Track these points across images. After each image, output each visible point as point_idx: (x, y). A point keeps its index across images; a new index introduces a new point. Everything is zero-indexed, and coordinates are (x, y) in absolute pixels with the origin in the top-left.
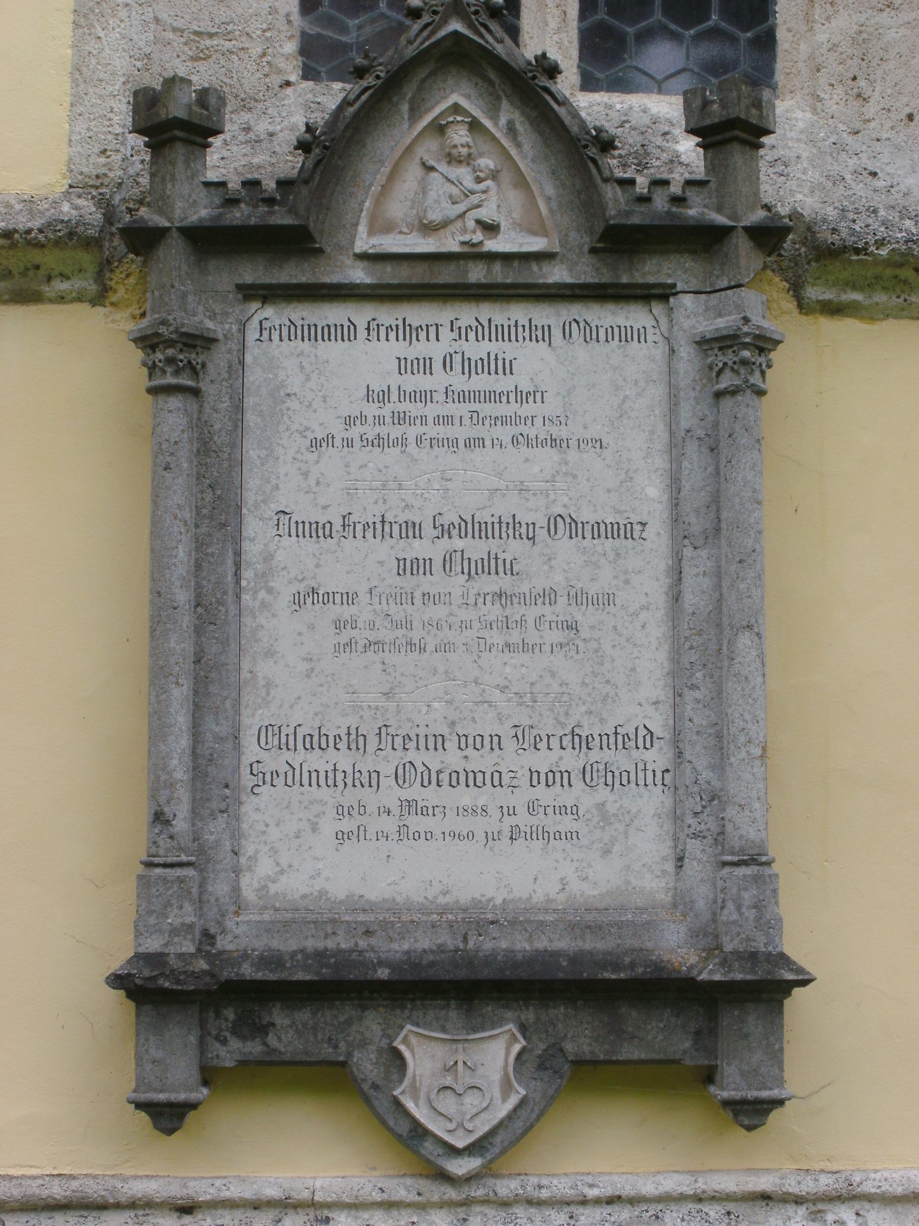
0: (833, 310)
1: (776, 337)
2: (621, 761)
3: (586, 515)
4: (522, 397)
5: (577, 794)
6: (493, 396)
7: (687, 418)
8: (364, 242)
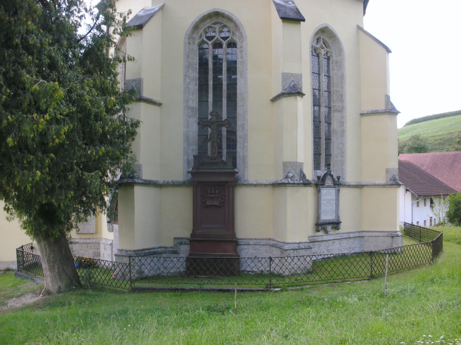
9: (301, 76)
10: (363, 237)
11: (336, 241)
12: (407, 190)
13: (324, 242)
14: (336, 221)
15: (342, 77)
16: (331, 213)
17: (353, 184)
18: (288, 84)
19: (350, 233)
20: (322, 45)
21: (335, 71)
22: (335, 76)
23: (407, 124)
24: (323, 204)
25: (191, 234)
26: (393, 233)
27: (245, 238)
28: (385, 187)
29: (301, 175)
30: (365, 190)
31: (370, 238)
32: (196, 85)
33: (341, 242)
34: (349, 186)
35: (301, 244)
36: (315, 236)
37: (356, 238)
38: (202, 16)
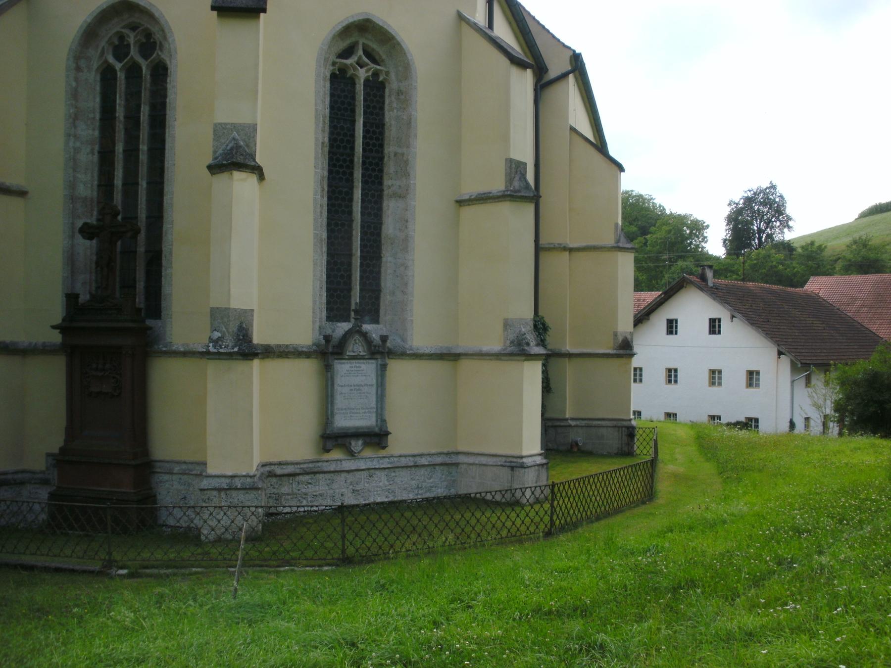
0: (392, 359)
1: (636, 327)
2: (371, 410)
3: (368, 384)
4: (363, 370)
5: (367, 414)
6: (359, 371)
7: (379, 373)
8: (348, 354)
9: (254, 127)
10: (457, 465)
11: (377, 472)
12: (780, 353)
13: (344, 475)
14: (377, 430)
15: (409, 124)
16: (365, 413)
17: (427, 351)
18: (224, 146)
19: (421, 455)
20: (360, 57)
21: (395, 111)
22: (393, 122)
23: (863, 215)
25: (61, 449)
26: (515, 460)
27: (168, 459)
28: (500, 360)
29: (238, 335)
30: (465, 365)
31: (471, 467)
32: (93, 154)
33: (393, 474)
35: (237, 480)
36: (318, 462)
37: (437, 467)
38: (98, 11)
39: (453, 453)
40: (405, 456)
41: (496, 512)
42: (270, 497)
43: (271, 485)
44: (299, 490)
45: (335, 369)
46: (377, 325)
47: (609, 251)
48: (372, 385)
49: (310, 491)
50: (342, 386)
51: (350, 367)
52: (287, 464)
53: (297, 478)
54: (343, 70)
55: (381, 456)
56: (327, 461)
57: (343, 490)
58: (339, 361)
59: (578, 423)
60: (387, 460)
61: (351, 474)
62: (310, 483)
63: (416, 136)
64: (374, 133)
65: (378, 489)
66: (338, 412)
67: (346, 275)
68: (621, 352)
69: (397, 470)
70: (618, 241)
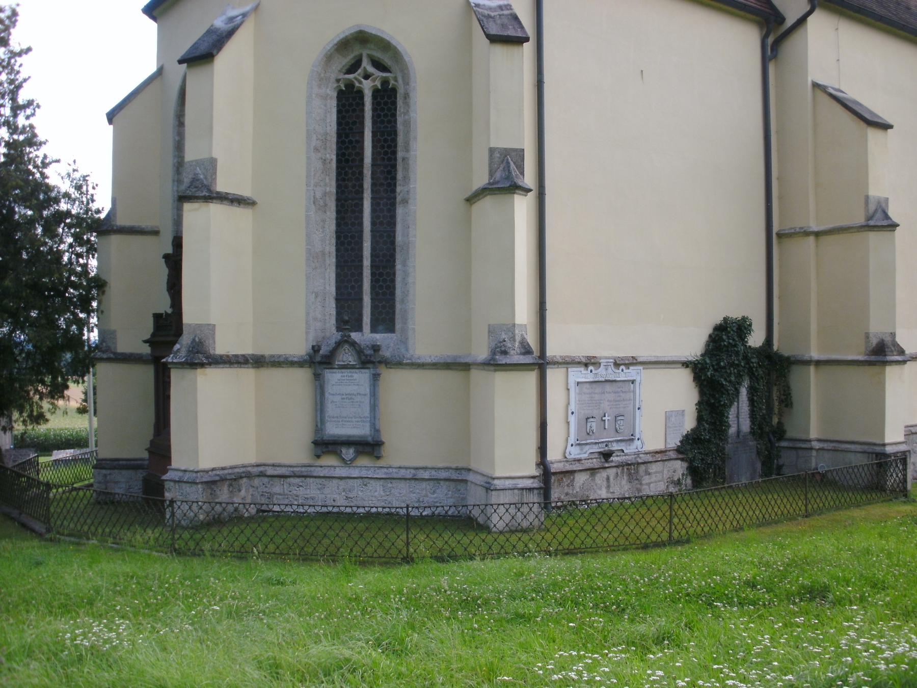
4: (356, 380)
8: (336, 363)
10: (465, 481)
11: (372, 482)
13: (335, 481)
16: (358, 422)
17: (429, 360)
24: (332, 402)
33: (390, 485)
34: (422, 366)
37: (442, 483)
39: (463, 469)
40: (406, 468)
41: (443, 535)
42: (262, 495)
43: (264, 484)
44: (290, 491)
45: (326, 378)
46: (390, 335)
47: (859, 232)
48: (365, 395)
49: (301, 493)
50: (333, 395)
51: (342, 376)
52: (280, 466)
53: (289, 480)
54: (350, 85)
55: (377, 465)
56: (321, 467)
57: (336, 496)
58: (331, 370)
59: (825, 445)
60: (385, 470)
61: (344, 481)
62: (301, 486)
63: (415, 138)
64: (386, 141)
65: (373, 499)
66: (329, 420)
67: (356, 286)
68: (873, 358)
69: (394, 481)
70: (870, 218)
